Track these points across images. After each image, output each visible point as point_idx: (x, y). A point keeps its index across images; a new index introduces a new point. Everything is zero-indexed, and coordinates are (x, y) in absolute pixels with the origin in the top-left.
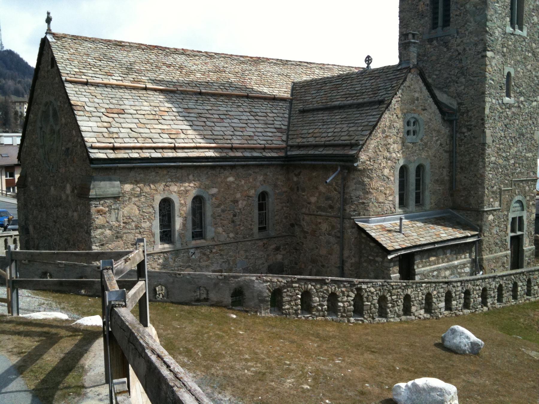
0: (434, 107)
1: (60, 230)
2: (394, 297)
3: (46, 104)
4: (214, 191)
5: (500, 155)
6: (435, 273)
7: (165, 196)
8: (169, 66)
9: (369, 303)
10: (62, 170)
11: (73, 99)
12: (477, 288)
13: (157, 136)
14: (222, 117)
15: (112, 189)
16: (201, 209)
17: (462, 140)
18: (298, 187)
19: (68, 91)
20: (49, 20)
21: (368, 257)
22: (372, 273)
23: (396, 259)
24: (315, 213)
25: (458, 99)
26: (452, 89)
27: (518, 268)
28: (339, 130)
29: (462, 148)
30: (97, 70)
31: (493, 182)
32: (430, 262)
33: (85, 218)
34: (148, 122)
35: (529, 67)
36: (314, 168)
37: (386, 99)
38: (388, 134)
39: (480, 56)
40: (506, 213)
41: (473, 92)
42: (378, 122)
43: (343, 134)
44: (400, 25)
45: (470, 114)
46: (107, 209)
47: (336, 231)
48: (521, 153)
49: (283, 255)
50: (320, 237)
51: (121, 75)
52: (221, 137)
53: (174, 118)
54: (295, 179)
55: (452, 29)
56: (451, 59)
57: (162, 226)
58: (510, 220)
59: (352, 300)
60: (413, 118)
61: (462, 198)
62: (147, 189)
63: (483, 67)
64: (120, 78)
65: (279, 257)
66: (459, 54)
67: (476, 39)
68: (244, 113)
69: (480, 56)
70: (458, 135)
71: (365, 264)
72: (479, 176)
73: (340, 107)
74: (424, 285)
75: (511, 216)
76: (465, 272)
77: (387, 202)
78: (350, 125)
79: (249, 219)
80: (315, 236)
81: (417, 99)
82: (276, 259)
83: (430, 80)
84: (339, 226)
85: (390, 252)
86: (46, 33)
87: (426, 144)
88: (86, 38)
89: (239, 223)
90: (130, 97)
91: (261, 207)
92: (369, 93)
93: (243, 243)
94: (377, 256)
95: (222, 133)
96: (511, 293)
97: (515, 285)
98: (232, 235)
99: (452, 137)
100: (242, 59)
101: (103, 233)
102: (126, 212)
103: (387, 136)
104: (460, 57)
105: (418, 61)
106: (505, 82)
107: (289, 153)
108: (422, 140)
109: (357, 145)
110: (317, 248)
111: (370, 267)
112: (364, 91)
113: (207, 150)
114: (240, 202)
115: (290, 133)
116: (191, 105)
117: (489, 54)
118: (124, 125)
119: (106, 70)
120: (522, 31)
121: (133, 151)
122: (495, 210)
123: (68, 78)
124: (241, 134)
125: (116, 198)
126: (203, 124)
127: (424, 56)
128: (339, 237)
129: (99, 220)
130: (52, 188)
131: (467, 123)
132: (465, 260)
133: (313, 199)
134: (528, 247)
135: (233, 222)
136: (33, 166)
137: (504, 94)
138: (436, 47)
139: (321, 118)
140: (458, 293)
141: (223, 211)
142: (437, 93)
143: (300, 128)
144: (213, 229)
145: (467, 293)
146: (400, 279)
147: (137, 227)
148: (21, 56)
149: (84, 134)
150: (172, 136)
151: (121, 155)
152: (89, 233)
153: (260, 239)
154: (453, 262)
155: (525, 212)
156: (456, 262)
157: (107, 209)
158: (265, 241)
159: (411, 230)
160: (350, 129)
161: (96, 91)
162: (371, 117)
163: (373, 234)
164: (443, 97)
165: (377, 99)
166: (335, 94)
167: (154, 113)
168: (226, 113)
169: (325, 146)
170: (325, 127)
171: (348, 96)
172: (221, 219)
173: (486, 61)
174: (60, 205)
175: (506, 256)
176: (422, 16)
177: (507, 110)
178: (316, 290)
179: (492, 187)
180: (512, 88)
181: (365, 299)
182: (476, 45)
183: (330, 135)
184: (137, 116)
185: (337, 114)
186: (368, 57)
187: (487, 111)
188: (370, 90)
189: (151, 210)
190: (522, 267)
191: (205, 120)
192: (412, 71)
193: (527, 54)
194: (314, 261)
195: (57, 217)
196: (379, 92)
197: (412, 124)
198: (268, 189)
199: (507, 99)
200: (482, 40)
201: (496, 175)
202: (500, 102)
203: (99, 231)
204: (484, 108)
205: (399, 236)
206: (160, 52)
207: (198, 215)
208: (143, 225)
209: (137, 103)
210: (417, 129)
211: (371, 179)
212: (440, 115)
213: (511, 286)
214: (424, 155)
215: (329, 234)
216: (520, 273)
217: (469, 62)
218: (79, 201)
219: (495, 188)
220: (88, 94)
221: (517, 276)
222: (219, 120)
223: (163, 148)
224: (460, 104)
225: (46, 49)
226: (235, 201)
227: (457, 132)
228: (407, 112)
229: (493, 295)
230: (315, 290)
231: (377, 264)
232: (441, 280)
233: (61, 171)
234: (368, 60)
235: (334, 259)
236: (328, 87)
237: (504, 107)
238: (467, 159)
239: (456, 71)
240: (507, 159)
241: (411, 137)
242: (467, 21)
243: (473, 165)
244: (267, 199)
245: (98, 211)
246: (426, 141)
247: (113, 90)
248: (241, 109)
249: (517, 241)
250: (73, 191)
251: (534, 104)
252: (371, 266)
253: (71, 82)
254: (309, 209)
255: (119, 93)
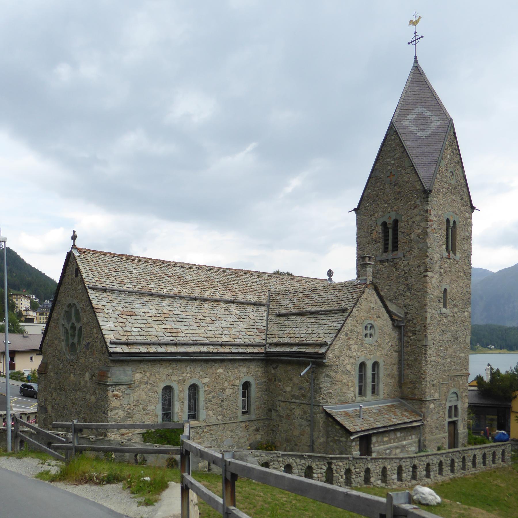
0: (386, 315)
1: (78, 410)
2: (357, 470)
3: (69, 306)
4: (206, 380)
5: (439, 355)
6: (388, 451)
7: (167, 384)
8: (170, 276)
9: (338, 475)
10: (82, 360)
11: (95, 303)
12: (422, 463)
13: (162, 334)
14: (213, 319)
15: (126, 378)
16: (195, 395)
17: (408, 342)
18: (275, 379)
19: (90, 297)
20: (74, 237)
21: (334, 438)
22: (337, 451)
23: (357, 440)
24: (290, 400)
25: (405, 309)
26: (400, 301)
27: (454, 448)
28: (310, 332)
29: (409, 349)
30: (114, 279)
31: (434, 377)
32: (383, 442)
33: (103, 401)
34: (154, 322)
35: (461, 285)
36: (289, 363)
37: (348, 308)
38: (350, 337)
39: (422, 275)
40: (444, 402)
41: (416, 304)
42: (342, 326)
43: (313, 335)
44: (357, 248)
45: (415, 321)
46: (121, 394)
47: (307, 415)
48: (456, 353)
49: (262, 435)
50: (294, 420)
51: (132, 284)
52: (213, 336)
53: (174, 319)
54: (273, 371)
55: (399, 253)
56: (398, 277)
57: (164, 409)
58: (448, 408)
59: (325, 472)
60: (370, 324)
61: (409, 390)
62: (153, 378)
63: (424, 284)
64: (131, 286)
65: (259, 437)
66: (406, 273)
67: (419, 262)
68: (231, 316)
69: (422, 275)
70: (406, 338)
71: (331, 443)
72: (422, 372)
73: (311, 313)
74: (380, 460)
75: (448, 405)
76: (412, 451)
77: (349, 392)
78: (319, 329)
79: (234, 404)
80: (289, 419)
81: (373, 309)
82: (256, 438)
83: (382, 293)
84: (309, 411)
85: (351, 434)
86: (72, 248)
87: (380, 345)
88: (104, 252)
89: (226, 408)
90: (140, 302)
91: (244, 395)
92: (334, 303)
93: (229, 425)
94: (342, 437)
95: (213, 332)
96: (450, 468)
97: (453, 461)
98: (220, 418)
99: (400, 340)
100: (228, 271)
101: (117, 414)
102: (135, 397)
103: (349, 339)
104: (406, 275)
105: (373, 277)
106: (442, 297)
107: (268, 350)
108: (376, 342)
109: (326, 344)
110: (291, 430)
111: (335, 446)
112: (330, 301)
113: (202, 347)
114: (227, 390)
115: (268, 333)
116: (188, 309)
117: (429, 274)
118: (135, 325)
119: (120, 279)
120: (455, 255)
121: (143, 346)
122: (435, 400)
123: (90, 286)
124: (229, 333)
125: (129, 385)
126: (198, 325)
127: (377, 273)
128: (309, 421)
129: (115, 403)
130: (72, 375)
131: (412, 329)
132: (412, 441)
133: (288, 389)
134: (462, 430)
135: (221, 406)
136: (54, 356)
137: (442, 306)
138: (386, 267)
139: (295, 321)
140: (407, 467)
141: (213, 397)
142: (388, 304)
143: (277, 329)
144: (205, 412)
145: (414, 467)
146: (360, 455)
147: (144, 409)
148: (18, 254)
149: (104, 332)
150: (173, 335)
151: (134, 349)
152: (105, 413)
153: (243, 422)
154: (402, 442)
155: (459, 401)
156: (404, 443)
157: (121, 394)
158: (247, 423)
159: (368, 416)
160: (320, 332)
161: (113, 297)
162: (337, 322)
163: (338, 419)
164: (392, 308)
165: (341, 308)
166: (305, 302)
167: (158, 315)
168: (216, 315)
169: (299, 345)
170: (298, 329)
171: (316, 304)
172: (212, 404)
173: (427, 280)
174: (79, 390)
175: (444, 438)
176: (376, 242)
177: (444, 319)
178: (296, 463)
179: (433, 381)
180: (448, 301)
181: (334, 472)
182: (419, 266)
183: (302, 335)
184: (146, 318)
185: (308, 319)
186: (330, 271)
187: (428, 320)
188: (335, 300)
189: (155, 395)
190: (457, 447)
191: (199, 321)
192: (369, 286)
193: (459, 274)
194: (288, 441)
195: (76, 399)
196: (342, 302)
197: (369, 329)
198: (251, 380)
199: (444, 310)
200: (424, 263)
201: (436, 371)
202: (439, 312)
203: (114, 412)
204: (426, 317)
205: (359, 421)
206: (163, 265)
207: (192, 400)
208: (149, 408)
209: (145, 307)
210: (373, 333)
211: (337, 372)
212: (391, 322)
213: (449, 462)
214: (378, 354)
215: (301, 418)
216: (456, 452)
217: (413, 280)
218: (97, 387)
219: (435, 382)
220: (106, 299)
221: (454, 453)
222: (210, 322)
223: (166, 344)
224: (406, 313)
225: (72, 261)
226: (224, 389)
227: (404, 335)
228: (365, 319)
229: (435, 469)
230: (295, 464)
231: (341, 444)
232: (392, 456)
233: (81, 361)
234: (330, 273)
235: (305, 439)
236: (299, 296)
237: (442, 316)
238: (412, 358)
239: (404, 287)
240: (444, 358)
241: (368, 340)
242: (412, 247)
243: (417, 363)
244: (249, 388)
245: (114, 396)
246: (380, 342)
247: (126, 296)
248: (228, 313)
249: (453, 424)
250: (92, 378)
251: (466, 314)
252: (337, 445)
253: (92, 289)
254: (285, 397)
255: (131, 299)
